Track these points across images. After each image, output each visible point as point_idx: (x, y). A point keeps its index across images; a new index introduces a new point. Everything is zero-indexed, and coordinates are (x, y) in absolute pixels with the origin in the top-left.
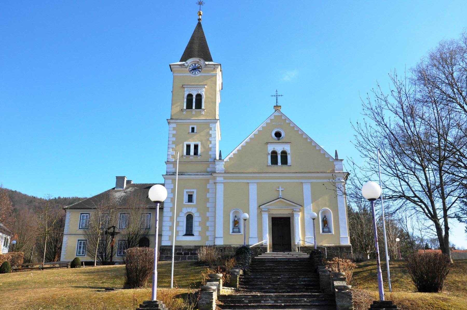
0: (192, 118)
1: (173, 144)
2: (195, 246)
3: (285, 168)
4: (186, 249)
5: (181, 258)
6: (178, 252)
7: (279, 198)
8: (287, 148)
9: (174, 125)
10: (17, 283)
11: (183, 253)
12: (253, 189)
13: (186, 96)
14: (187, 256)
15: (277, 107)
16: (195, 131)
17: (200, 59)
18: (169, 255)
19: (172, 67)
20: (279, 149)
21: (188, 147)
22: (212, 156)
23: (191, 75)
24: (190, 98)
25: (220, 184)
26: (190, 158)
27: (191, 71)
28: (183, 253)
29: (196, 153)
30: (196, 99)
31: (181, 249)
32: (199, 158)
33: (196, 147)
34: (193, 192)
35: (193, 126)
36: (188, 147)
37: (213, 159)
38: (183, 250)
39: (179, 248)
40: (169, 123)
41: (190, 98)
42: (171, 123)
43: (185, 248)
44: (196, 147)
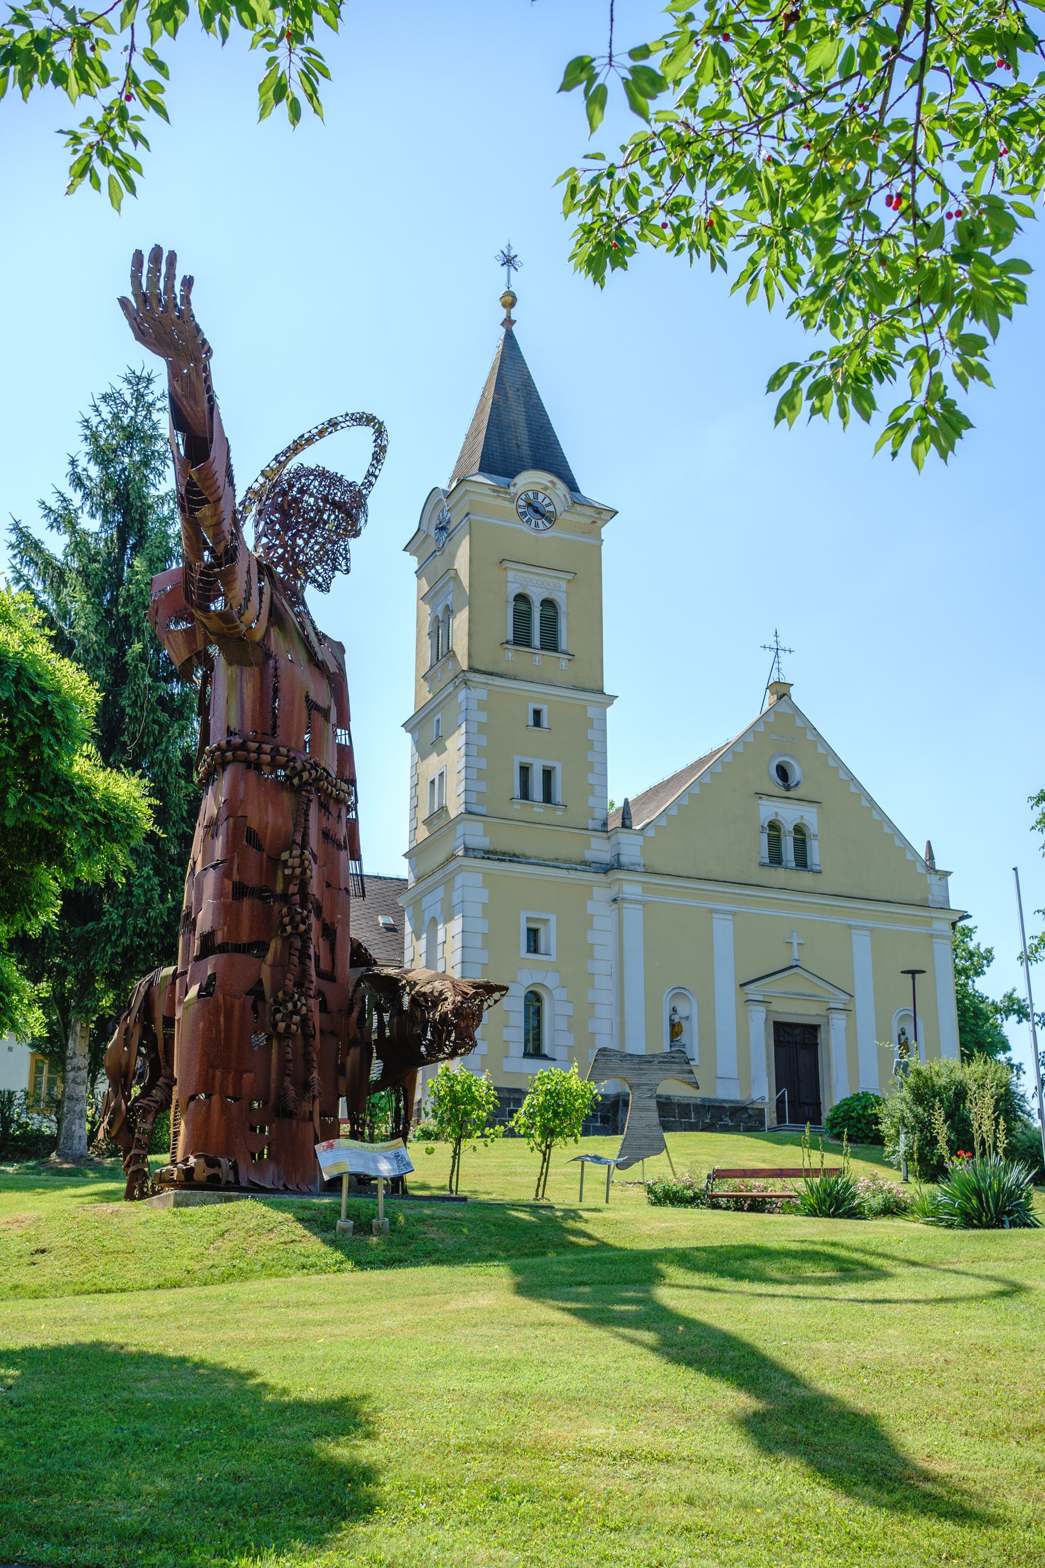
0: (1011, 272)
3: (804, 879)
7: (791, 967)
8: (809, 816)
12: (723, 931)
13: (511, 599)
15: (780, 691)
16: (545, 721)
20: (789, 814)
21: (525, 770)
22: (599, 815)
23: (525, 527)
24: (523, 607)
25: (633, 906)
29: (548, 798)
33: (548, 774)
34: (546, 921)
36: (525, 770)
37: (600, 823)
44: (548, 774)
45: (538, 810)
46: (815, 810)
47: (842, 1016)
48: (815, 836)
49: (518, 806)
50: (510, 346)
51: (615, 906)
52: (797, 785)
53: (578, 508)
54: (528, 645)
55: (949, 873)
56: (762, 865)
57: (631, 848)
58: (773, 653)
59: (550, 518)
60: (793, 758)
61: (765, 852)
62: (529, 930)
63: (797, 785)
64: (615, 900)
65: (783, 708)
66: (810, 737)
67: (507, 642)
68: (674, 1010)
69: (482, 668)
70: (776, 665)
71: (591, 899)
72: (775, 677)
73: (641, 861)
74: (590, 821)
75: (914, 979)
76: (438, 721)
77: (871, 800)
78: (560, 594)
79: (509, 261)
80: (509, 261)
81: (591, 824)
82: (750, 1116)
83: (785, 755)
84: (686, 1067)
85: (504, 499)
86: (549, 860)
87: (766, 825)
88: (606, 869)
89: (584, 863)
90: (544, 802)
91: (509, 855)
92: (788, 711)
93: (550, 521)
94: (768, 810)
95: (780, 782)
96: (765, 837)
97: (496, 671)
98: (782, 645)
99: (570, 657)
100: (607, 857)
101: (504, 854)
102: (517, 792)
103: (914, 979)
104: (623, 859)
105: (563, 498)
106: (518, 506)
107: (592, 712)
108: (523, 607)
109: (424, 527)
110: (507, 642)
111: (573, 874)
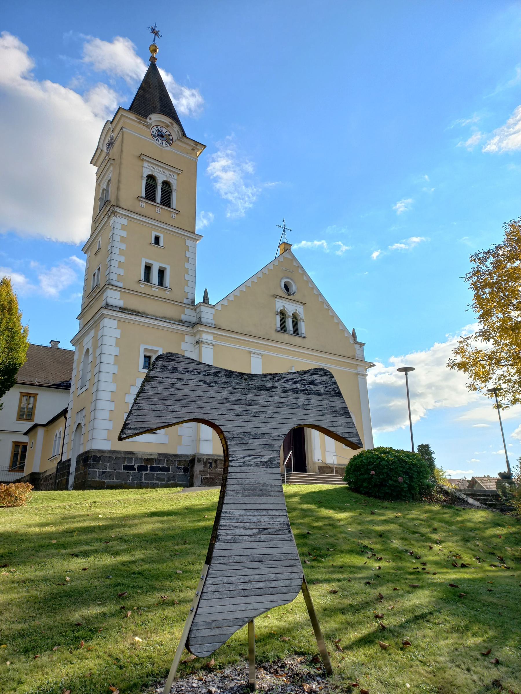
2: (159, 454)
3: (297, 340)
4: (141, 459)
5: (131, 477)
6: (126, 464)
8: (300, 310)
10: (450, 602)
11: (136, 467)
14: (144, 473)
15: (286, 247)
17: (173, 122)
18: (108, 470)
20: (290, 308)
21: (148, 268)
22: (190, 296)
23: (155, 142)
24: (151, 182)
26: (153, 289)
28: (136, 467)
29: (161, 282)
31: (132, 458)
32: (168, 293)
33: (161, 272)
35: (158, 234)
36: (148, 268)
37: (190, 301)
38: (136, 460)
39: (130, 456)
42: (119, 215)
43: (140, 456)
44: (161, 272)
45: (156, 290)
46: (302, 307)
48: (303, 320)
49: (143, 288)
51: (197, 346)
52: (294, 293)
53: (185, 139)
55: (364, 344)
56: (277, 331)
59: (169, 142)
60: (292, 280)
61: (278, 325)
62: (145, 357)
63: (294, 293)
64: (197, 342)
65: (286, 255)
70: (283, 235)
71: (184, 341)
72: (283, 240)
73: (213, 322)
74: (185, 299)
75: (406, 374)
76: (100, 242)
77: (328, 306)
78: (174, 180)
79: (155, 32)
80: (155, 32)
81: (186, 301)
84: (334, 403)
85: (144, 125)
86: (159, 317)
87: (279, 311)
88: (193, 325)
90: (158, 285)
92: (289, 257)
94: (280, 304)
98: (286, 227)
99: (177, 212)
100: (194, 320)
101: (132, 311)
102: (142, 277)
103: (406, 374)
104: (203, 320)
105: (177, 133)
106: (152, 132)
108: (151, 182)
109: (100, 146)
111: (173, 326)
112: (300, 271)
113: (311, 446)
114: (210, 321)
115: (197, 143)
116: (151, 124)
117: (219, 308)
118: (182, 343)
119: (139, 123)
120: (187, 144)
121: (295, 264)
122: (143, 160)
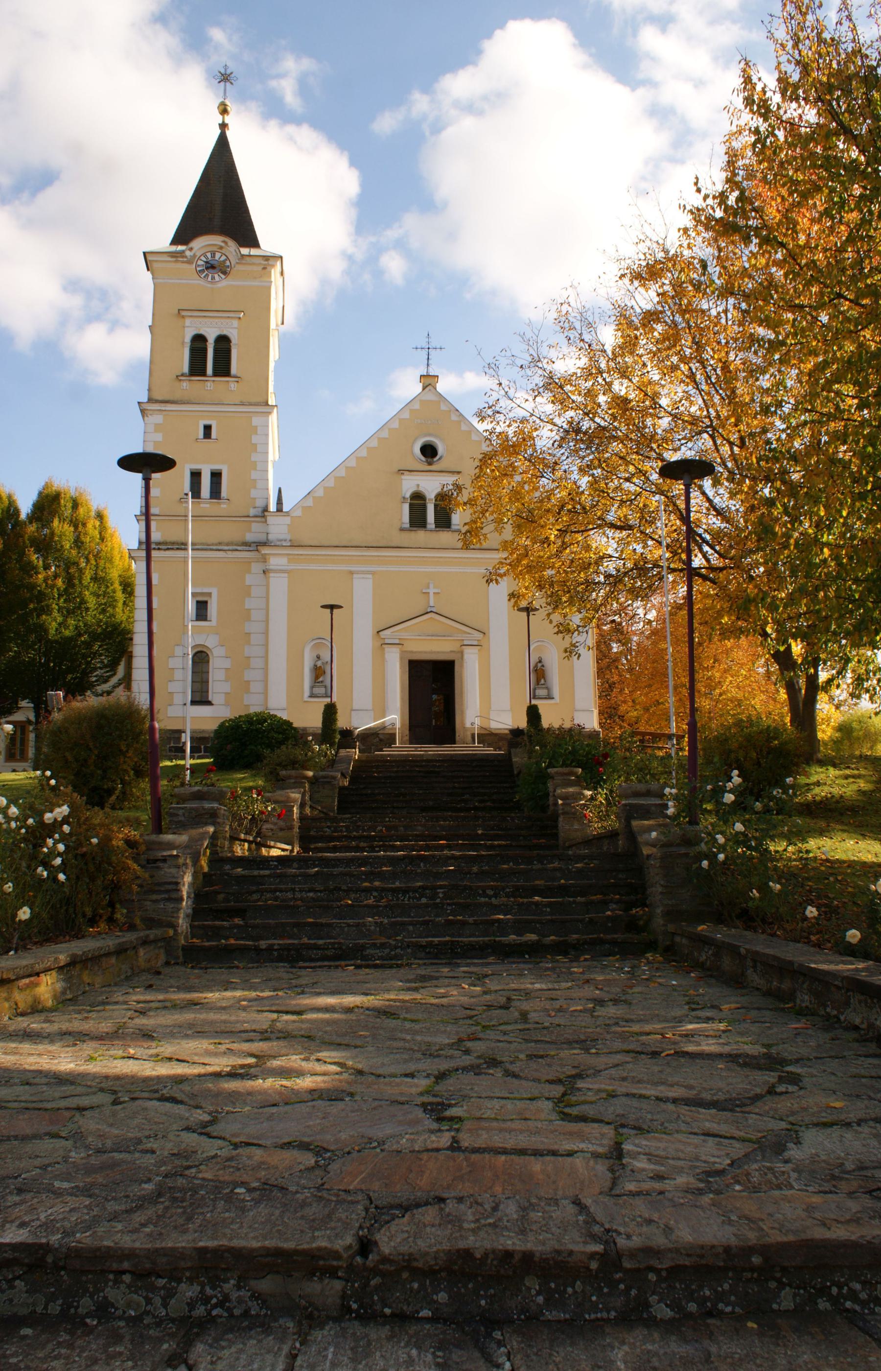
1: (156, 431)
9: (158, 419)
13: (188, 339)
15: (428, 381)
19: (149, 258)
22: (260, 503)
23: (202, 282)
24: (199, 345)
27: (202, 271)
29: (216, 493)
30: (216, 351)
33: (216, 476)
34: (210, 594)
40: (143, 412)
41: (199, 345)
44: (216, 476)
45: (207, 505)
47: (475, 650)
50: (222, 148)
54: (203, 373)
56: (402, 530)
57: (278, 528)
58: (425, 352)
66: (454, 417)
67: (182, 375)
68: (318, 657)
69: (160, 398)
71: (249, 572)
73: (288, 537)
82: (381, 740)
83: (430, 435)
85: (183, 262)
87: (408, 495)
89: (245, 544)
90: (211, 498)
91: (177, 544)
93: (225, 273)
95: (423, 458)
96: (406, 507)
97: (171, 398)
101: (173, 543)
107: (256, 421)
110: (182, 375)
111: (230, 554)
112: (454, 417)
113: (462, 704)
114: (282, 537)
115: (267, 258)
116: (195, 256)
117: (299, 513)
118: (247, 576)
119: (176, 261)
120: (254, 264)
121: (443, 407)
122: (183, 317)
